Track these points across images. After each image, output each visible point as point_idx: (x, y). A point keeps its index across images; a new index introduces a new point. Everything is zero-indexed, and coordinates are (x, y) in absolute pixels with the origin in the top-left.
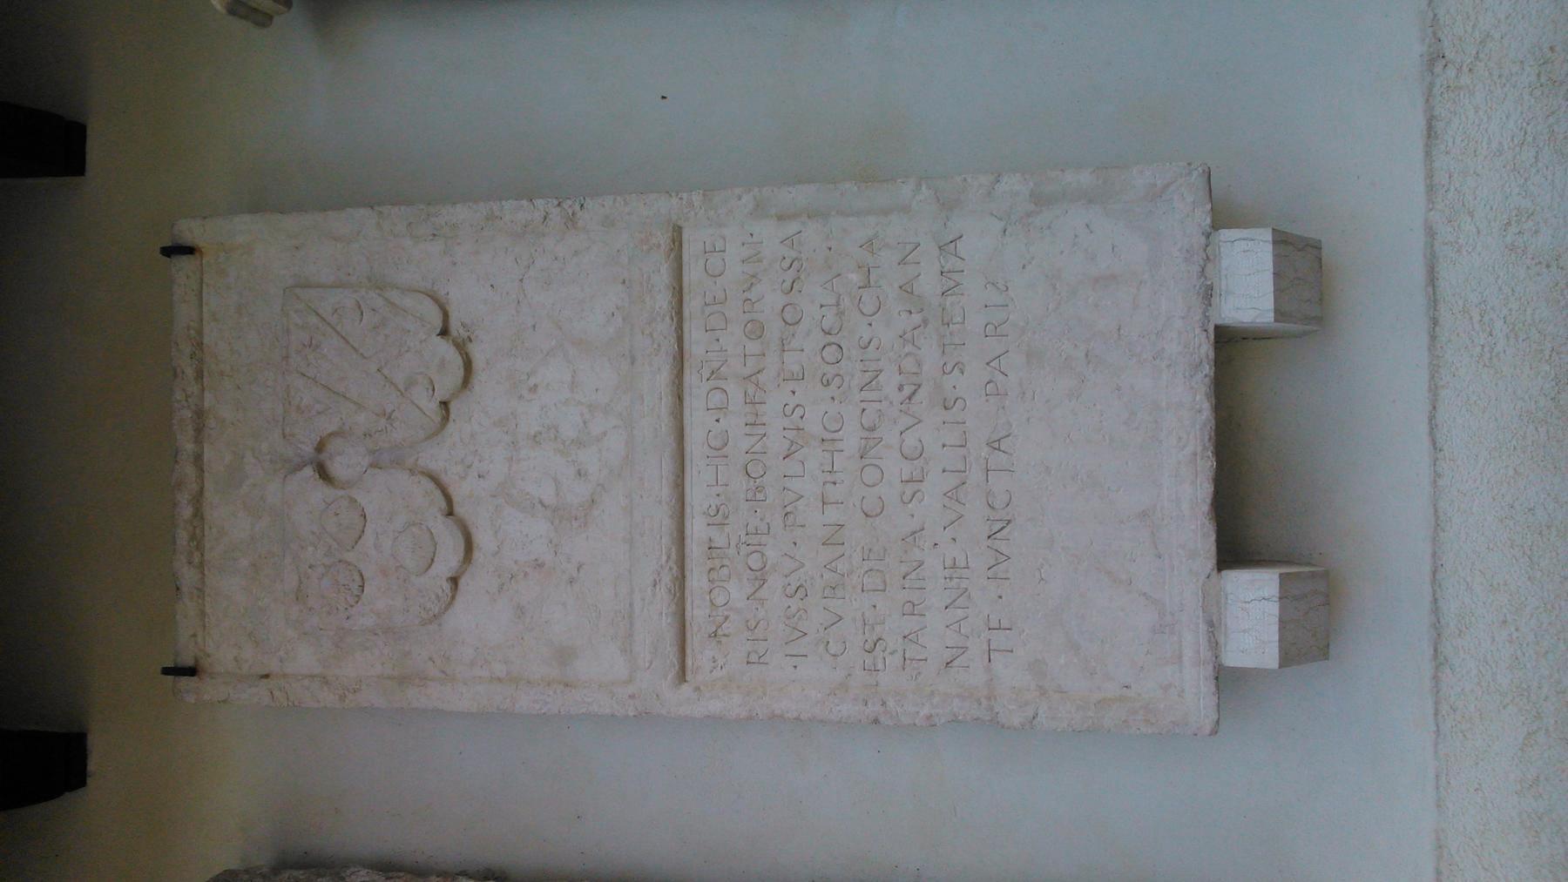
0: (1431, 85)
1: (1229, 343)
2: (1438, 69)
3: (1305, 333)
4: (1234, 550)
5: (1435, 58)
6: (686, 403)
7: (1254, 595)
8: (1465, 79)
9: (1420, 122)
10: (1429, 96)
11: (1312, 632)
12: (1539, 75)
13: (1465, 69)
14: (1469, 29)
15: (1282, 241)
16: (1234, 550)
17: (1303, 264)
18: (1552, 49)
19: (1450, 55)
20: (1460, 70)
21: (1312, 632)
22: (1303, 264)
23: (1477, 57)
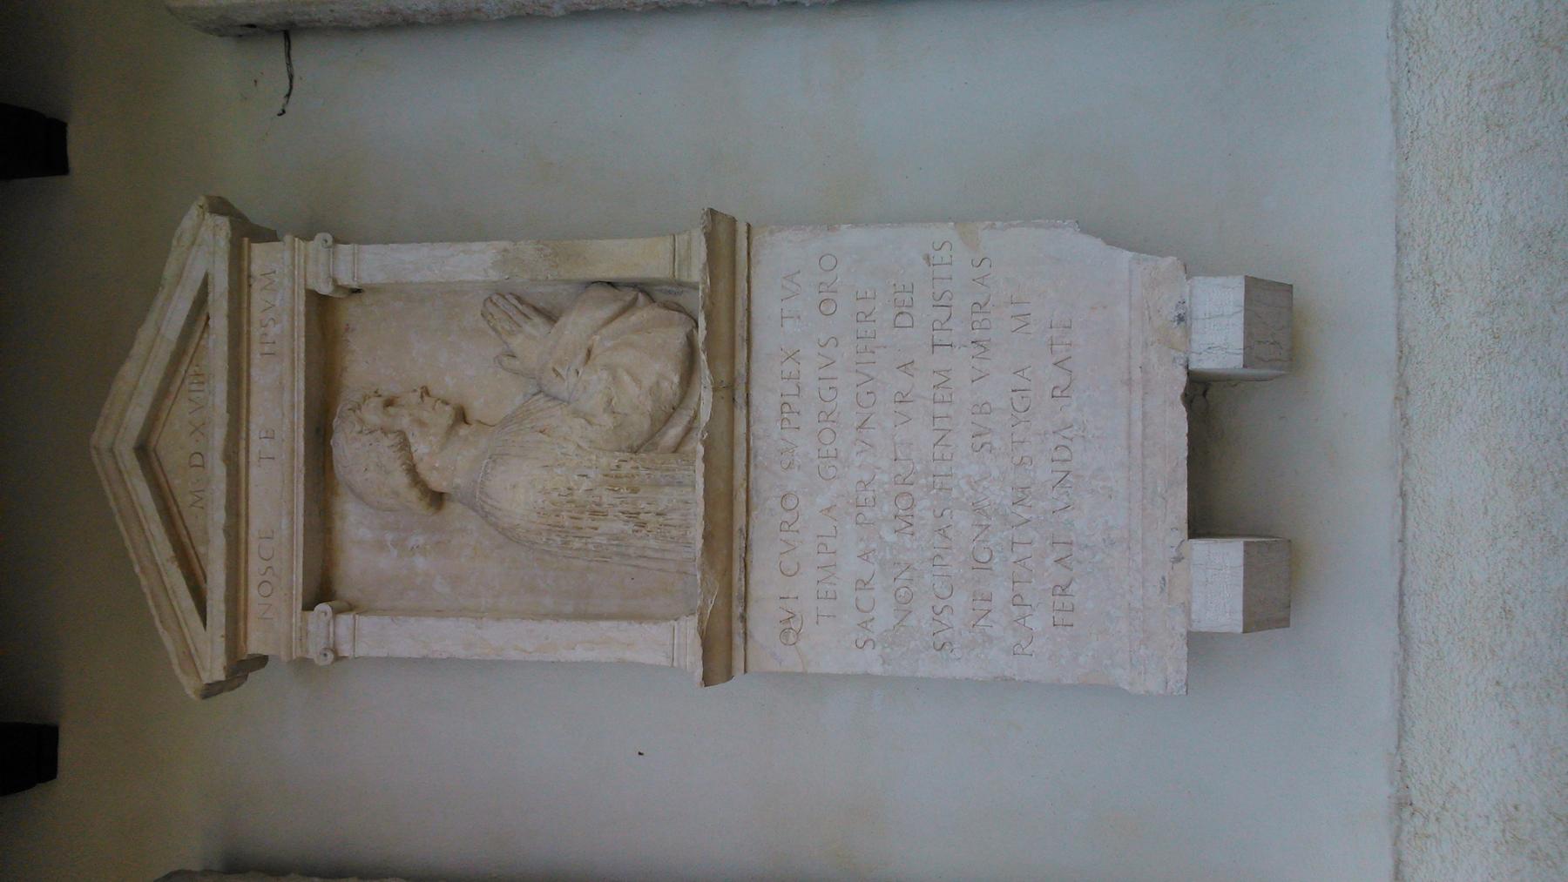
0: (1399, 829)
1: (1201, 392)
2: (1406, 814)
3: (1277, 377)
4: (1201, 524)
5: (1402, 804)
6: (754, 514)
7: (1224, 559)
8: (1432, 828)
9: (1388, 863)
10: (1396, 839)
11: (1273, 602)
12: (1504, 831)
13: (1432, 818)
14: (1436, 779)
15: (1252, 285)
16: (1201, 524)
17: (1276, 314)
18: (1516, 808)
19: (1418, 804)
20: (1427, 818)
21: (1273, 602)
22: (1276, 314)
23: (1444, 808)
